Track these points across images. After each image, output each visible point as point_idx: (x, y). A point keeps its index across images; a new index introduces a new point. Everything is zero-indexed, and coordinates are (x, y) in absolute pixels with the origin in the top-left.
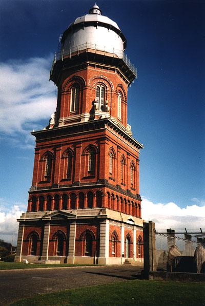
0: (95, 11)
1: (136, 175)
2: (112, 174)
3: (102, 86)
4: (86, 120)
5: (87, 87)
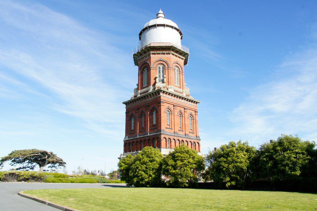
0: (160, 15)
1: (195, 123)
2: (169, 125)
3: (162, 66)
4: (151, 91)
5: (151, 69)
